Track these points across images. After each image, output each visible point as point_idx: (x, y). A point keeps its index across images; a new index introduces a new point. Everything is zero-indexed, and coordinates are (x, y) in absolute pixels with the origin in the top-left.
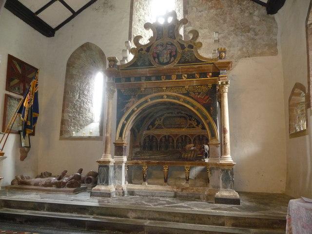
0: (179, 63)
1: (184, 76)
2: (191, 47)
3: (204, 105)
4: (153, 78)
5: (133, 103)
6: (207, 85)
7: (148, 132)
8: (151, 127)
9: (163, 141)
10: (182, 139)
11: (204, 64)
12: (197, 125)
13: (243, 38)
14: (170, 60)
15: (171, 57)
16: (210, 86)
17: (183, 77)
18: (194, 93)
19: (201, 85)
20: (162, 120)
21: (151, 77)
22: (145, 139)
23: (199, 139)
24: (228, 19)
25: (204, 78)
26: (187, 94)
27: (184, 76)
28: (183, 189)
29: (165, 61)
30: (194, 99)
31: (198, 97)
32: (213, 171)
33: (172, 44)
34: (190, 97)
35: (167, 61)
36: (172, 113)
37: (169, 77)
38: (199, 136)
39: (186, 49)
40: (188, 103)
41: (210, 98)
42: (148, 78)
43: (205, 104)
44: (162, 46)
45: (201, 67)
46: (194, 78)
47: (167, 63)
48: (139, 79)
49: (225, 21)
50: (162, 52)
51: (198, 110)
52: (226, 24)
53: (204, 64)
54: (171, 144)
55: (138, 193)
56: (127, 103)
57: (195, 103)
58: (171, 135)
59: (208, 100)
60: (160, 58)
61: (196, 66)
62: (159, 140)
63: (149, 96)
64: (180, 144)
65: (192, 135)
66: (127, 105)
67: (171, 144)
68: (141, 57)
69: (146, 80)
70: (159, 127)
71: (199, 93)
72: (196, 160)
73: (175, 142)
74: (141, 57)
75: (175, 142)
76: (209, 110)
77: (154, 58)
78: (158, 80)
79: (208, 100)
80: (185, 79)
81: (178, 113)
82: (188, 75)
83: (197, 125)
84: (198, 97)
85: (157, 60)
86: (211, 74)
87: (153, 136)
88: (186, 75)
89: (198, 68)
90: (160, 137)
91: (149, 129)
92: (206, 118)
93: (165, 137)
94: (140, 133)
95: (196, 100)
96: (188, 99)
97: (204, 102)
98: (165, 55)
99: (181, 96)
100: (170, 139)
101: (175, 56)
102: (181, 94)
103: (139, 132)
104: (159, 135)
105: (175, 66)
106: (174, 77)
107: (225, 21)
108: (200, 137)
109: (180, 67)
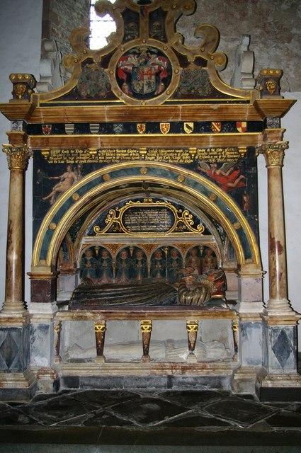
0: (175, 96)
1: (188, 126)
2: (201, 62)
3: (229, 191)
4: (118, 128)
5: (72, 182)
6: (237, 150)
7: (91, 239)
8: (97, 228)
9: (124, 257)
10: (163, 253)
11: (230, 102)
12: (195, 226)
13: (278, 52)
14: (157, 89)
15: (157, 81)
16: (243, 149)
17: (186, 129)
18: (209, 163)
19: (224, 148)
20: (120, 217)
21: (112, 124)
22: (84, 255)
23: (198, 254)
24: (250, 13)
25: (229, 132)
26: (193, 166)
27: (188, 126)
28: (184, 369)
29: (146, 90)
30: (208, 177)
31: (218, 172)
32: (248, 329)
33: (160, 54)
34: (199, 172)
35: (150, 91)
36: (142, 201)
37: (153, 127)
38: (197, 248)
39: (192, 67)
40: (195, 185)
41: (242, 176)
42: (107, 128)
43: (230, 187)
44: (138, 55)
45: (227, 108)
46: (209, 130)
47: (151, 95)
48: (82, 128)
49: (244, 15)
50: (137, 68)
51: (217, 200)
52: (245, 22)
53: (230, 102)
54: (140, 265)
55: (86, 382)
56: (58, 181)
57: (211, 186)
58: (141, 247)
59: (237, 181)
60: (134, 83)
61: (215, 106)
62: (114, 257)
63: (109, 168)
64: (159, 266)
65: (184, 247)
66: (56, 188)
67: (140, 265)
68: (88, 78)
69: (100, 132)
70: (115, 229)
71: (219, 165)
72: (210, 306)
73: (149, 260)
74: (88, 78)
75: (149, 260)
76: (240, 203)
77: (120, 82)
78: (130, 133)
79: (237, 181)
80: (188, 132)
81: (154, 201)
82: (196, 124)
83: (195, 226)
84: (218, 172)
85: (126, 86)
86: (244, 125)
87: (101, 249)
88: (191, 125)
89: (220, 109)
90: (118, 251)
91: (92, 234)
92: (233, 219)
93: (127, 249)
94: (76, 244)
95: (214, 180)
96: (195, 175)
97: (230, 184)
98: (146, 77)
99: (180, 169)
100: (139, 254)
101: (167, 82)
102: (179, 165)
103: (73, 241)
104: (114, 247)
105: (166, 103)
106: (165, 127)
107: (244, 15)
108: (199, 251)
109: (180, 106)
